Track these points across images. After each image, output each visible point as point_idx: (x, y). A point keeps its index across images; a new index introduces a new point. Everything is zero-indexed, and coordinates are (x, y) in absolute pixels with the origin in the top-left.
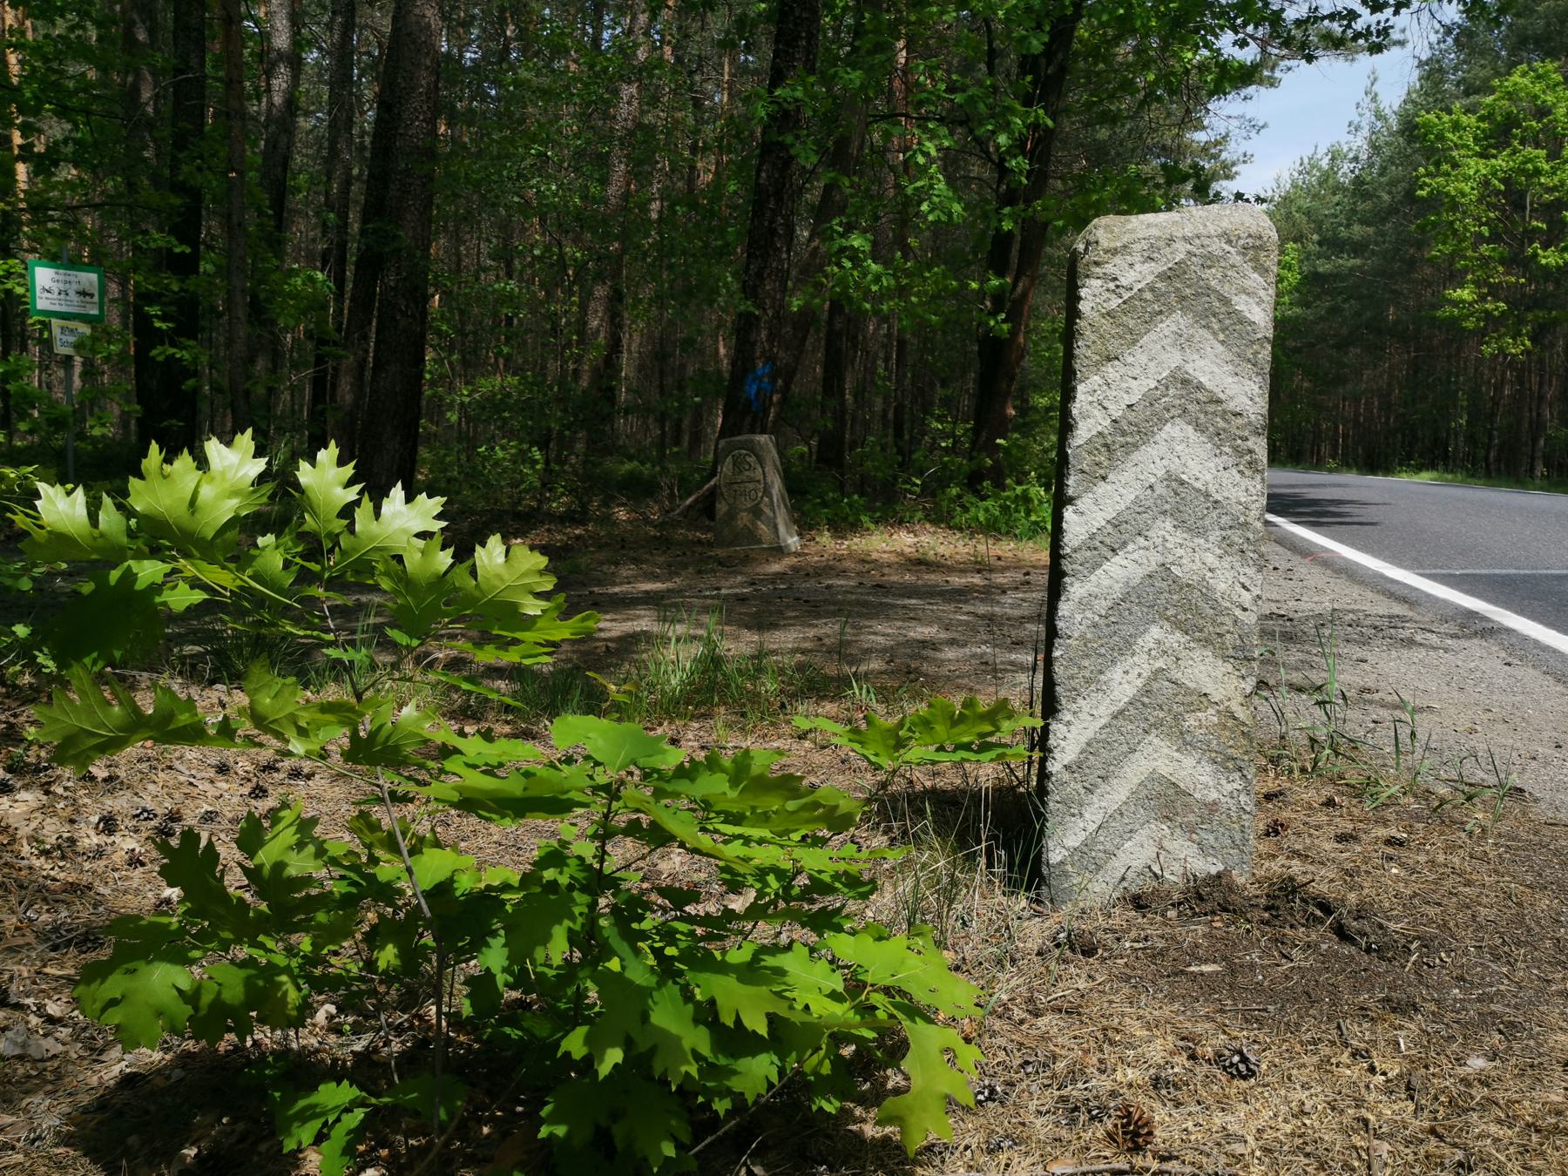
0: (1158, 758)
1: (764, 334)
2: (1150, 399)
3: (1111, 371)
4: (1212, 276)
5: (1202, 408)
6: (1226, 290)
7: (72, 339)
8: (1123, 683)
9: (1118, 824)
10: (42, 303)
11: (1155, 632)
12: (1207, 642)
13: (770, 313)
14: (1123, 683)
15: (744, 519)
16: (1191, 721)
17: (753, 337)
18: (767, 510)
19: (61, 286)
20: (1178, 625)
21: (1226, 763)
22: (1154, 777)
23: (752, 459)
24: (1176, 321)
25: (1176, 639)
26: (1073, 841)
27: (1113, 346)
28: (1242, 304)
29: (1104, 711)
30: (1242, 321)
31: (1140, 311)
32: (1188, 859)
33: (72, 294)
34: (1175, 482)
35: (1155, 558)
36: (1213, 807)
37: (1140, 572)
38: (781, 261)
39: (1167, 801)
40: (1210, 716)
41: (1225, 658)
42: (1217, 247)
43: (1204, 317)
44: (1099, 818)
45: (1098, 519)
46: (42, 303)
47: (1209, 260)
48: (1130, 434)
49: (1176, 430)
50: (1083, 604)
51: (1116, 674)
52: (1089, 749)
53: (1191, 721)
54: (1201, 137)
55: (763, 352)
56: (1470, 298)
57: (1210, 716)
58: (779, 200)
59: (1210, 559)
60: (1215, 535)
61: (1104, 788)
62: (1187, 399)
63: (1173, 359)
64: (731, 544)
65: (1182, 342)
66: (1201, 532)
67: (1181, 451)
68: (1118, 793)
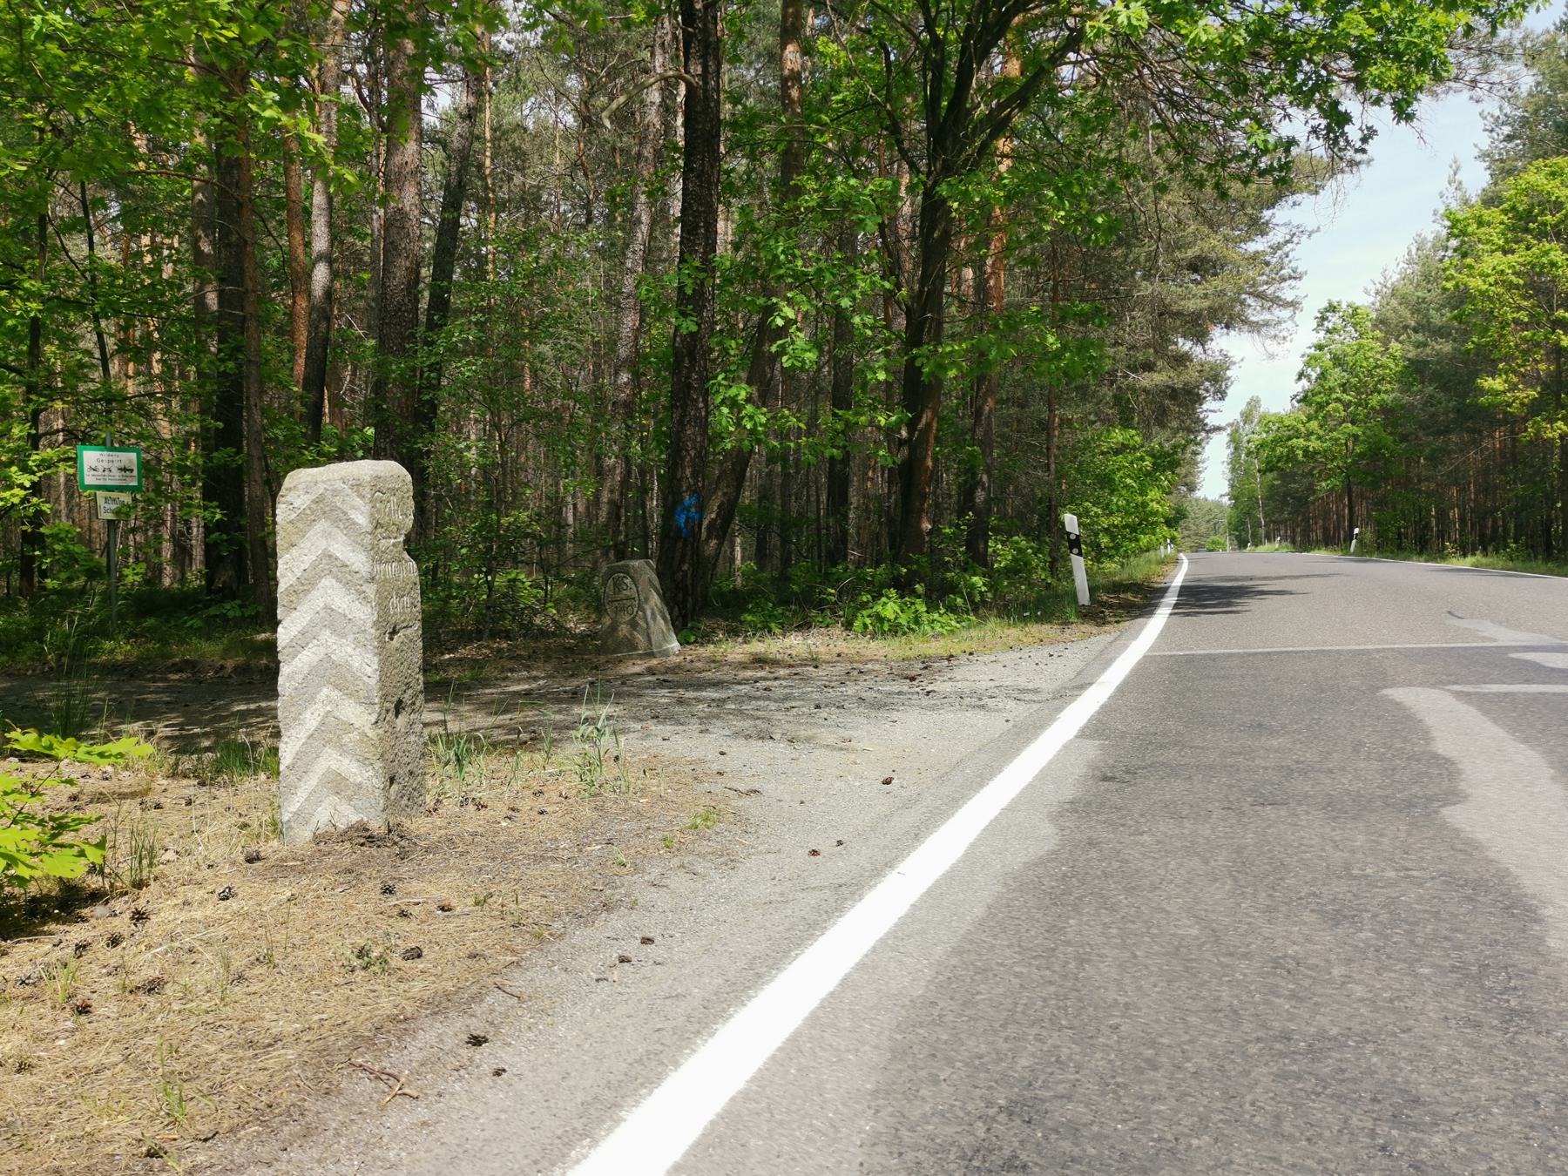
0: (331, 761)
1: (688, 472)
2: (314, 565)
3: (294, 551)
4: (338, 501)
5: (340, 570)
6: (344, 508)
7: (113, 507)
8: (311, 719)
9: (314, 799)
10: (89, 479)
11: (325, 690)
12: (350, 695)
13: (692, 453)
14: (311, 719)
15: (624, 630)
16: (346, 739)
17: (679, 475)
18: (641, 623)
19: (106, 465)
20: (337, 687)
21: (364, 761)
22: (329, 771)
23: (628, 581)
24: (322, 525)
25: (336, 694)
26: (293, 809)
27: (294, 539)
28: (353, 515)
29: (303, 735)
30: (354, 523)
31: (307, 519)
32: (349, 816)
33: (114, 470)
34: (328, 608)
35: (323, 651)
36: (359, 786)
37: (316, 658)
38: (699, 409)
39: (337, 784)
40: (355, 736)
41: (361, 704)
42: (339, 485)
43: (336, 521)
44: (305, 795)
45: (294, 631)
46: (89, 479)
47: (336, 493)
48: (307, 584)
49: (327, 582)
50: (290, 677)
51: (308, 714)
52: (298, 757)
53: (346, 739)
54: (1258, 245)
55: (689, 488)
56: (1501, 388)
57: (355, 736)
58: (693, 359)
59: (349, 650)
60: (351, 637)
61: (306, 777)
62: (331, 566)
63: (323, 544)
64: (615, 652)
65: (327, 535)
66: (344, 636)
67: (330, 593)
68: (312, 780)
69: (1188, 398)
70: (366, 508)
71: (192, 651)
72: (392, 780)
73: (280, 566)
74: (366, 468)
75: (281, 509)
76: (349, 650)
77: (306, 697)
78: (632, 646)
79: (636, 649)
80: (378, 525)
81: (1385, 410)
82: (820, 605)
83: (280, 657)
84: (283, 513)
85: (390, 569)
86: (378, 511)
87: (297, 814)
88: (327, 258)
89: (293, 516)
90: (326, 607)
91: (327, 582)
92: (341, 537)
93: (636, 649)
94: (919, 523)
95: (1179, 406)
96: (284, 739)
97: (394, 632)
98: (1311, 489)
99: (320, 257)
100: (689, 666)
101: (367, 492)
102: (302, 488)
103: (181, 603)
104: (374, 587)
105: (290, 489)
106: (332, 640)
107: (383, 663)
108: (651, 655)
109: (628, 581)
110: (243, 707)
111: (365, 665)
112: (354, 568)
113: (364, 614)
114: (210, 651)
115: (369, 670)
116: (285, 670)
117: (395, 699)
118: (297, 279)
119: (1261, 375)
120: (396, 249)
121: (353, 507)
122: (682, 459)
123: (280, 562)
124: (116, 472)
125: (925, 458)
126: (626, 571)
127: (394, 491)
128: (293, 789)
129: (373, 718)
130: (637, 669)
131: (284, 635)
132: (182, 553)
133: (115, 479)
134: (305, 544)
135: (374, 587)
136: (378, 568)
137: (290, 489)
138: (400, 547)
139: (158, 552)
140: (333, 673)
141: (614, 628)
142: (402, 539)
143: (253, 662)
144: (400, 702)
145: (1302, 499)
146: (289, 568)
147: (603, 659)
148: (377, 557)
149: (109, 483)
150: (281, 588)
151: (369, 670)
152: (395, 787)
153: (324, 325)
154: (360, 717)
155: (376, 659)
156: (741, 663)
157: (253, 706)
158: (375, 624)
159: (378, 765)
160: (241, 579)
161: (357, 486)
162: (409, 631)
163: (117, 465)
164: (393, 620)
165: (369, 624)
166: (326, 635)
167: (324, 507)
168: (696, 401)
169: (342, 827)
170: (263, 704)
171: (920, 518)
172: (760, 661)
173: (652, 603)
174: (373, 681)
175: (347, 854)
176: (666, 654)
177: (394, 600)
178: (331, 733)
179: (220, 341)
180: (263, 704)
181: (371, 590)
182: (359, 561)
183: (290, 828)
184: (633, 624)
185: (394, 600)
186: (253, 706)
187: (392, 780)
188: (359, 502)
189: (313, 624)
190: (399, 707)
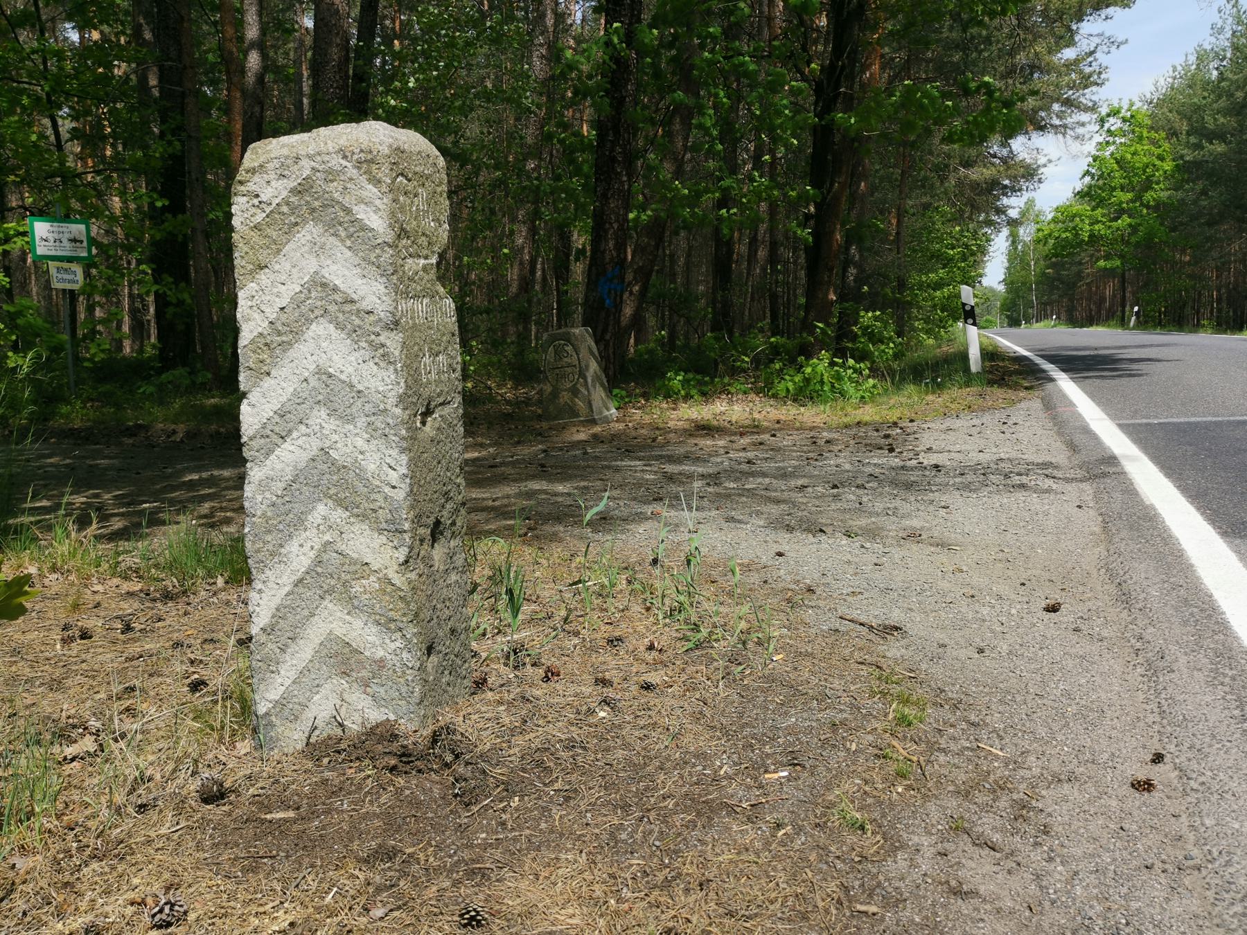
0: (332, 621)
1: (611, 244)
2: (297, 302)
3: (264, 277)
6: (347, 201)
8: (299, 555)
11: (321, 509)
12: (363, 517)
14: (299, 555)
15: (565, 397)
18: (583, 390)
20: (340, 503)
21: (387, 625)
22: (331, 638)
23: (569, 348)
24: (309, 232)
25: (339, 515)
26: (274, 694)
27: (263, 256)
28: (361, 212)
29: (287, 580)
30: (364, 228)
31: (284, 221)
32: (365, 711)
35: (315, 444)
36: (381, 663)
38: (622, 183)
39: (343, 659)
40: (372, 583)
41: (381, 531)
42: (336, 162)
43: (332, 226)
44: (293, 674)
45: (267, 410)
46: (40, 251)
47: (331, 175)
48: (286, 333)
49: (320, 329)
50: (263, 486)
51: (293, 547)
52: (280, 613)
53: (357, 588)
54: (1069, 54)
57: (372, 583)
59: (360, 443)
60: (362, 421)
61: (293, 648)
62: (323, 299)
63: (311, 265)
64: (556, 418)
65: (318, 249)
66: (350, 419)
67: (326, 348)
69: (992, 189)
70: (384, 203)
71: (150, 413)
72: (430, 650)
73: (242, 302)
74: (376, 134)
75: (239, 206)
76: (360, 443)
77: (289, 519)
78: (574, 413)
79: (577, 415)
80: (402, 233)
81: (1158, 206)
82: (734, 372)
83: (246, 453)
84: (242, 212)
85: (421, 307)
86: (402, 209)
87: (280, 704)
88: (260, 45)
89: (260, 217)
90: (319, 371)
91: (320, 329)
92: (342, 253)
93: (577, 415)
94: (827, 294)
95: (983, 200)
96: (258, 585)
97: (428, 413)
98: (1079, 275)
99: (253, 45)
100: (634, 434)
101: (384, 174)
102: (270, 171)
103: (138, 369)
104: (399, 337)
105: (253, 171)
106: (331, 424)
107: (414, 463)
108: (593, 422)
109: (569, 348)
110: (195, 477)
111: (386, 466)
112: (365, 305)
113: (382, 383)
114: (164, 419)
115: (393, 477)
116: (255, 474)
117: (431, 521)
118: (232, 65)
119: (1057, 170)
120: (326, 25)
121: (361, 201)
122: (606, 231)
123: (241, 295)
124: (66, 243)
125: (833, 232)
126: (568, 339)
127: (423, 178)
128: (272, 664)
129: (402, 554)
130: (582, 436)
131: (251, 417)
132: (139, 329)
133: (66, 250)
134: (281, 265)
135: (399, 337)
136: (404, 305)
137: (253, 171)
138: (433, 274)
139: (119, 327)
140: (333, 481)
141: (555, 394)
142: (434, 260)
143: (203, 428)
144: (438, 523)
145: (1087, 279)
146: (257, 305)
147: (545, 425)
148: (402, 287)
149: (59, 253)
150: (245, 338)
151: (393, 477)
152: (434, 659)
153: (257, 109)
154: (379, 553)
155: (404, 459)
156: (685, 430)
157: (205, 475)
158: (401, 399)
159: (411, 630)
160: (197, 350)
161: (367, 162)
162: (447, 410)
163: (67, 235)
164: (426, 393)
165: (392, 400)
166: (319, 416)
167: (312, 202)
168: (620, 174)
169: (354, 726)
170: (216, 473)
171: (828, 290)
172: (705, 429)
173: (591, 370)
174: (400, 495)
175: (373, 794)
176: (607, 420)
177: (427, 360)
178: (332, 578)
179: (163, 122)
180: (216, 473)
181: (393, 342)
182: (372, 293)
183: (271, 725)
184: (575, 392)
185: (427, 360)
186: (205, 475)
187: (430, 650)
188: (371, 190)
189: (298, 400)
190: (436, 531)
